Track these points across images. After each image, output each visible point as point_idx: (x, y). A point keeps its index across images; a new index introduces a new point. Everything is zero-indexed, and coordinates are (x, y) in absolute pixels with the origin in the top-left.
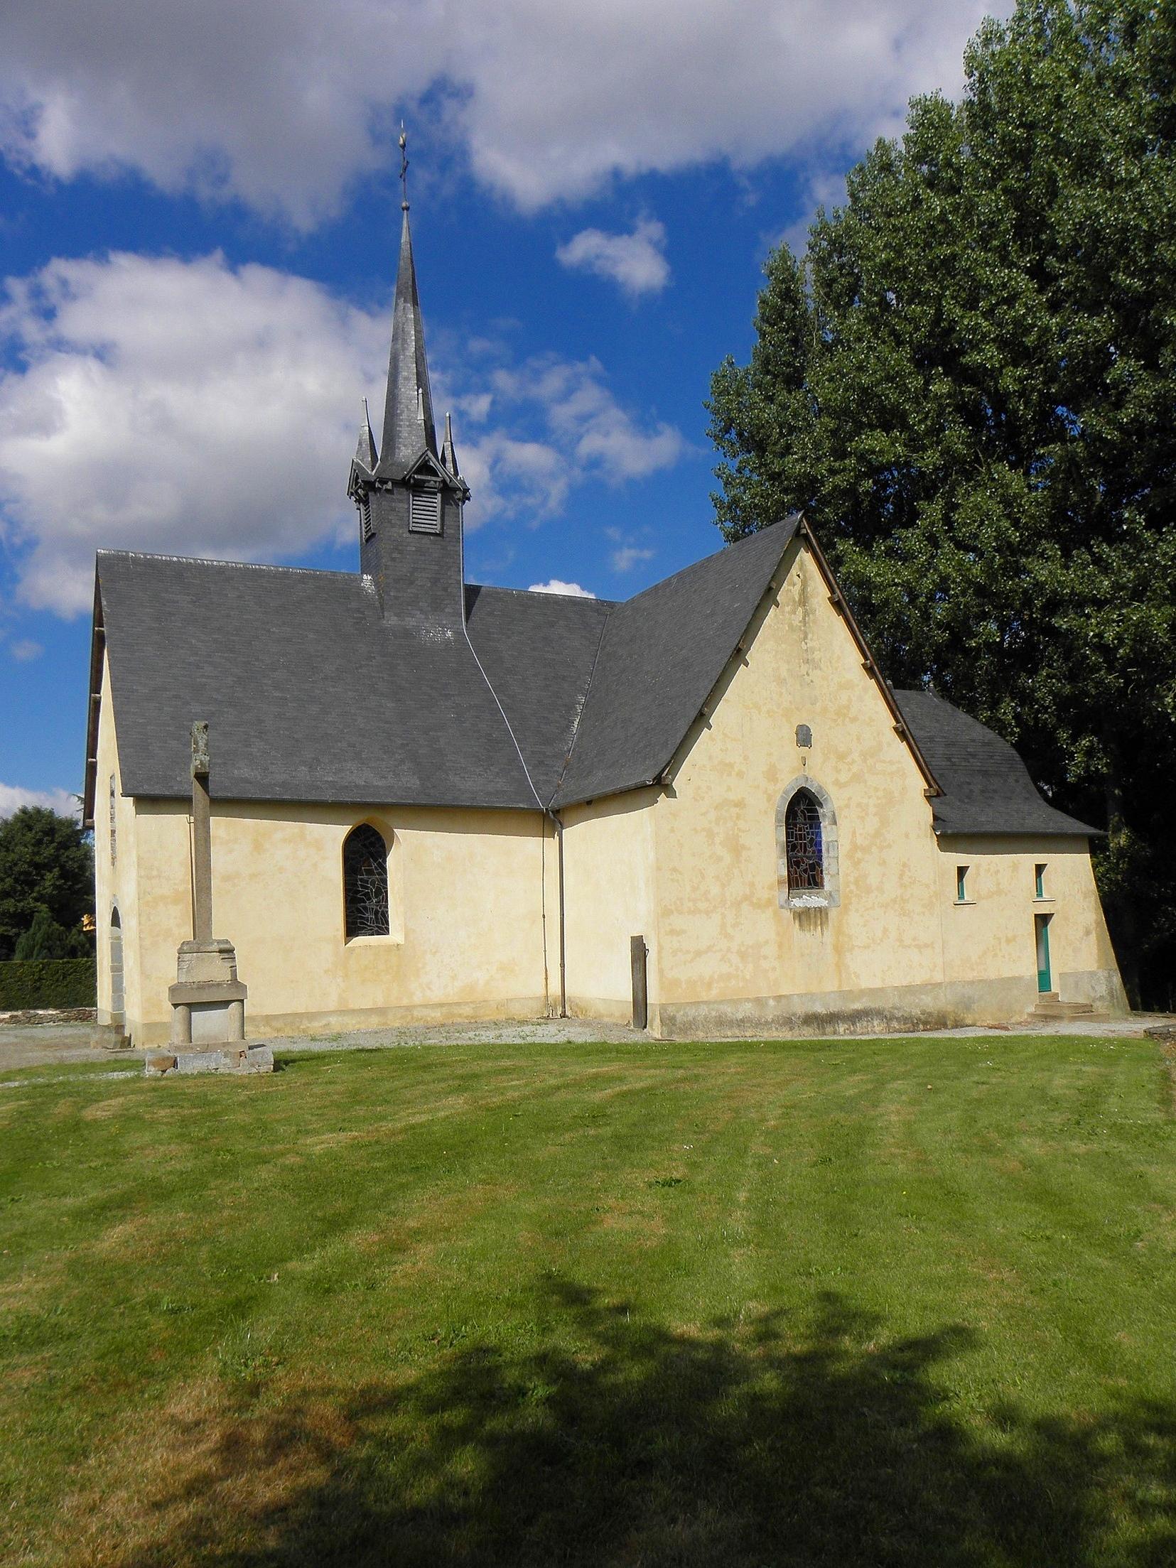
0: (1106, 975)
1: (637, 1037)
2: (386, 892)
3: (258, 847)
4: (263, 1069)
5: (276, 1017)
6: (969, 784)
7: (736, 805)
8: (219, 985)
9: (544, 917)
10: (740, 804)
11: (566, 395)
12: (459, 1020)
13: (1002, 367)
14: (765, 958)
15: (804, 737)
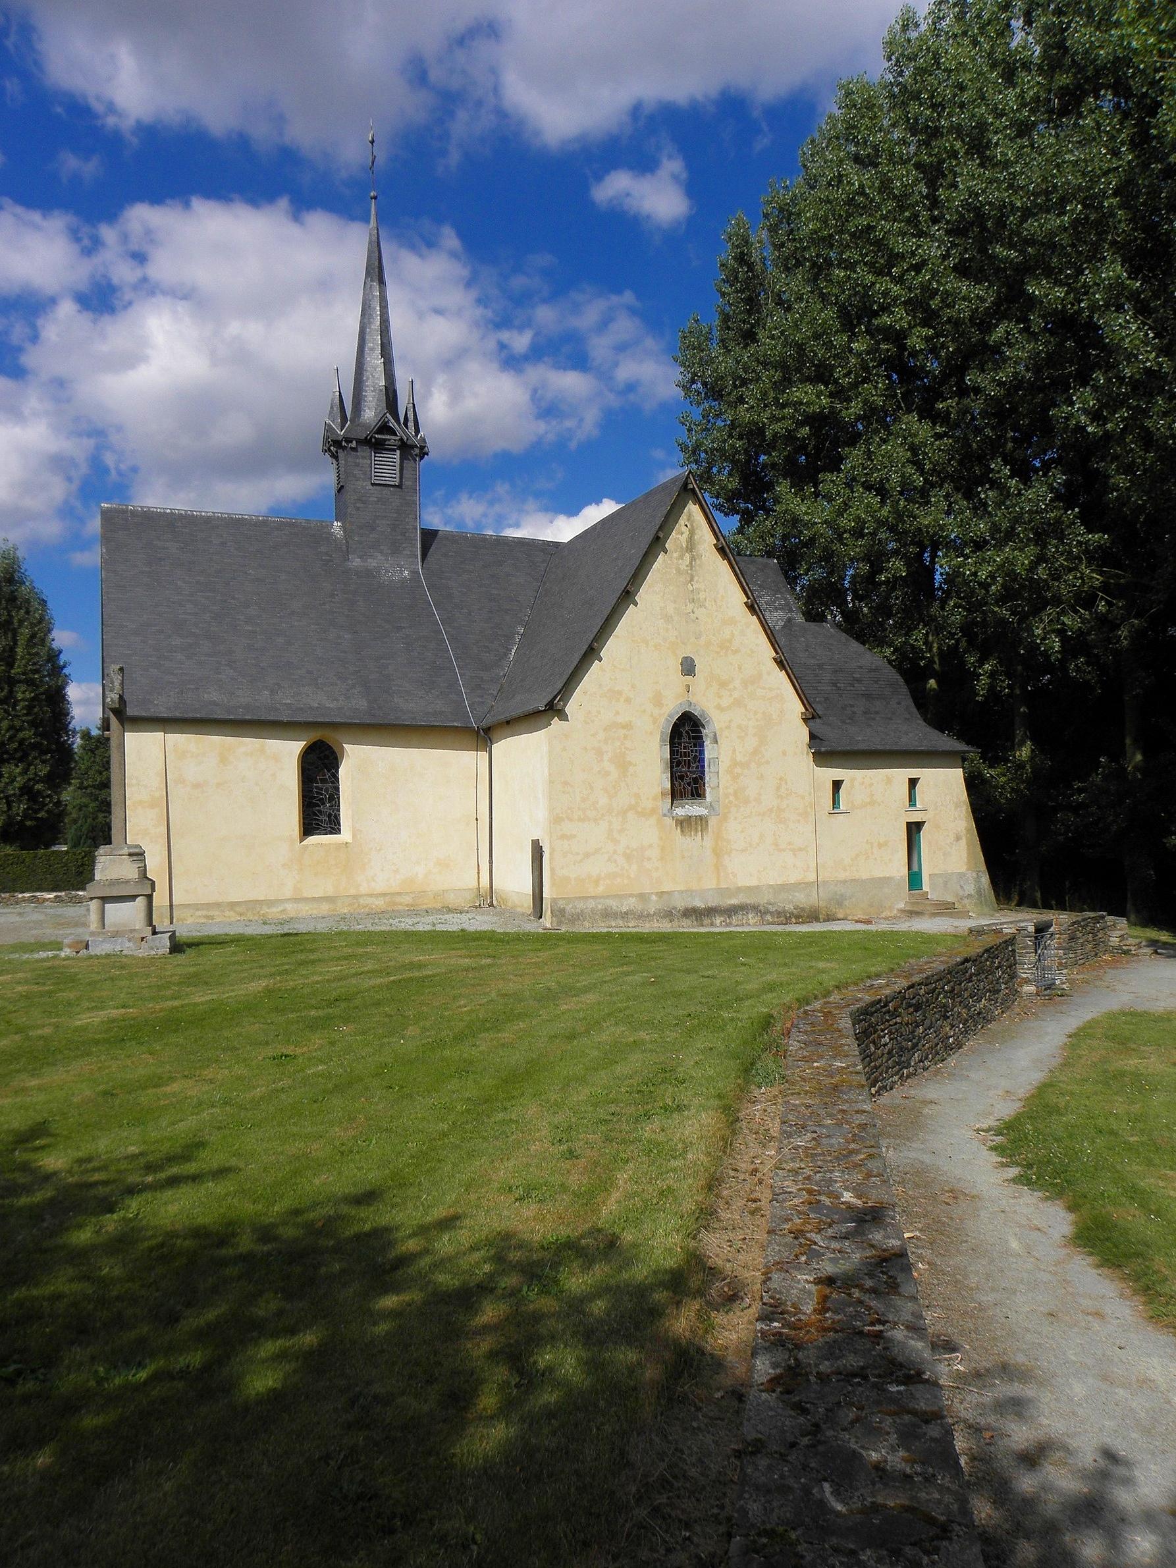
0: (974, 875)
1: (532, 927)
2: (339, 798)
3: (223, 760)
4: (161, 952)
5: (238, 903)
6: (852, 706)
7: (623, 727)
8: (127, 882)
9: (477, 819)
10: (628, 726)
11: (605, 324)
12: (400, 907)
13: (911, 327)
14: (649, 859)
15: (688, 667)
